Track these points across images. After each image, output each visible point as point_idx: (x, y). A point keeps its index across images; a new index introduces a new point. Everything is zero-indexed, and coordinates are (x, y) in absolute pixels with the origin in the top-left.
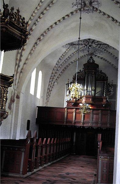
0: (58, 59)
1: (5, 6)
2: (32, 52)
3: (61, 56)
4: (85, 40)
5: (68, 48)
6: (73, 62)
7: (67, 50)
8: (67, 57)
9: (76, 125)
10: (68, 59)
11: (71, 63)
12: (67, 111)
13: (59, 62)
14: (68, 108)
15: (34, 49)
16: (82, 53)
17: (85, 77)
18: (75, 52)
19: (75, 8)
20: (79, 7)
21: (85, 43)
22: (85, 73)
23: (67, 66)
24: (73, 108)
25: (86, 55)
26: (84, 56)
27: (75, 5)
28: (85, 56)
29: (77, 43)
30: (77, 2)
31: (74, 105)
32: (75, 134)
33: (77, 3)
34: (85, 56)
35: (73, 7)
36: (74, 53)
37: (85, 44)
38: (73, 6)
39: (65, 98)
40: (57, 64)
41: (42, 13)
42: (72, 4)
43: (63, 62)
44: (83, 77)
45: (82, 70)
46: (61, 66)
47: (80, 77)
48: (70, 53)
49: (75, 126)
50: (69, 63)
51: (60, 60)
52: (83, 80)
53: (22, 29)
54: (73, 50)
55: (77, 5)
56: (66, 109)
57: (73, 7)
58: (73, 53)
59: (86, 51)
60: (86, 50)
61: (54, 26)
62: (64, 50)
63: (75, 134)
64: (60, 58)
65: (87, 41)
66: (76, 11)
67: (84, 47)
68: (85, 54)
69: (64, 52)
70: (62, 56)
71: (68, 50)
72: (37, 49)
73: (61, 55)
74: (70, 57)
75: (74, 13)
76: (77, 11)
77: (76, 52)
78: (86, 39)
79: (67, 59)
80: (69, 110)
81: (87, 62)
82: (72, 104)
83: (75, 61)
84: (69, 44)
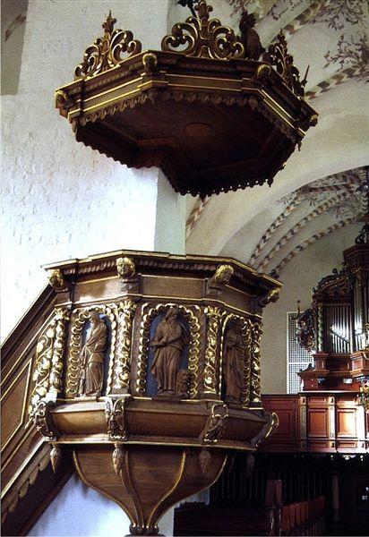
0: (257, 239)
1: (109, 25)
2: (196, 217)
3: (269, 230)
4: (349, 172)
5: (292, 203)
6: (305, 245)
7: (288, 208)
8: (285, 231)
9: (341, 451)
10: (289, 236)
11: (297, 251)
12: (307, 406)
13: (260, 250)
14: (309, 396)
15: (201, 208)
16: (335, 215)
17: (352, 292)
18: (311, 215)
19: (335, 67)
20: (349, 63)
21: (349, 182)
22: (353, 278)
23: (286, 260)
24: (327, 395)
25: (347, 223)
26: (340, 225)
27: (335, 59)
28: (344, 224)
29: (320, 185)
30: (343, 49)
31: (324, 385)
32: (335, 480)
33: (341, 52)
34: (344, 224)
35: (326, 66)
36: (310, 219)
37: (347, 186)
38: (326, 63)
39: (288, 363)
40: (253, 256)
41: (290, 27)
42: (326, 57)
43: (273, 250)
44: (345, 291)
45: (340, 268)
46: (266, 262)
47: (336, 293)
48: (298, 217)
49: (339, 456)
50: (291, 250)
51: (293, 234)
52: (346, 301)
53: (233, 63)
54: (308, 209)
55: (340, 60)
56: (302, 398)
57: (326, 66)
58: (305, 219)
59: (347, 209)
60: (345, 205)
61: (333, 84)
62: (279, 210)
63: (335, 480)
64: (264, 237)
65: (357, 177)
66: (338, 78)
67: (344, 194)
68: (345, 218)
69: (278, 214)
70: (272, 231)
71: (292, 208)
72: (209, 207)
73: (268, 225)
74: (295, 231)
75: (345, 79)
76: (342, 77)
77: (315, 215)
78: (351, 170)
79: (285, 237)
80: (315, 403)
81: (354, 244)
82: (319, 380)
83: (310, 244)
84: (335, 175)
